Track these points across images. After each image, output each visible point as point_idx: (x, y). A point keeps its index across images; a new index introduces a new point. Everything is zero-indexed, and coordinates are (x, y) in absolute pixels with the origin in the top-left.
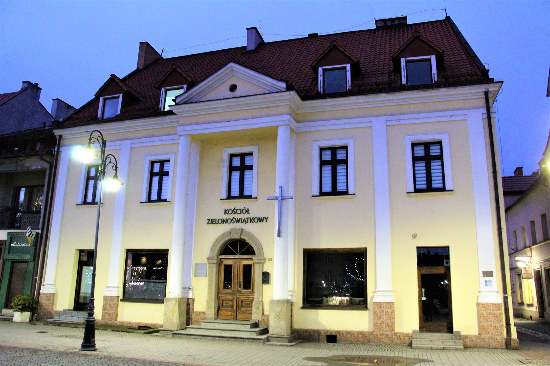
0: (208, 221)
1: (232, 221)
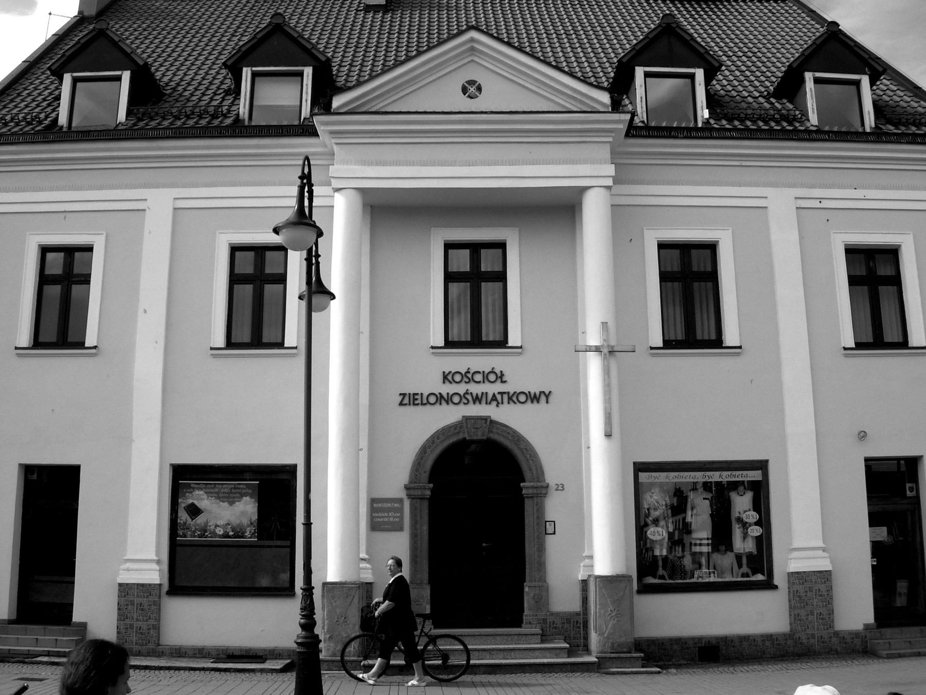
0: (400, 398)
1: (465, 398)
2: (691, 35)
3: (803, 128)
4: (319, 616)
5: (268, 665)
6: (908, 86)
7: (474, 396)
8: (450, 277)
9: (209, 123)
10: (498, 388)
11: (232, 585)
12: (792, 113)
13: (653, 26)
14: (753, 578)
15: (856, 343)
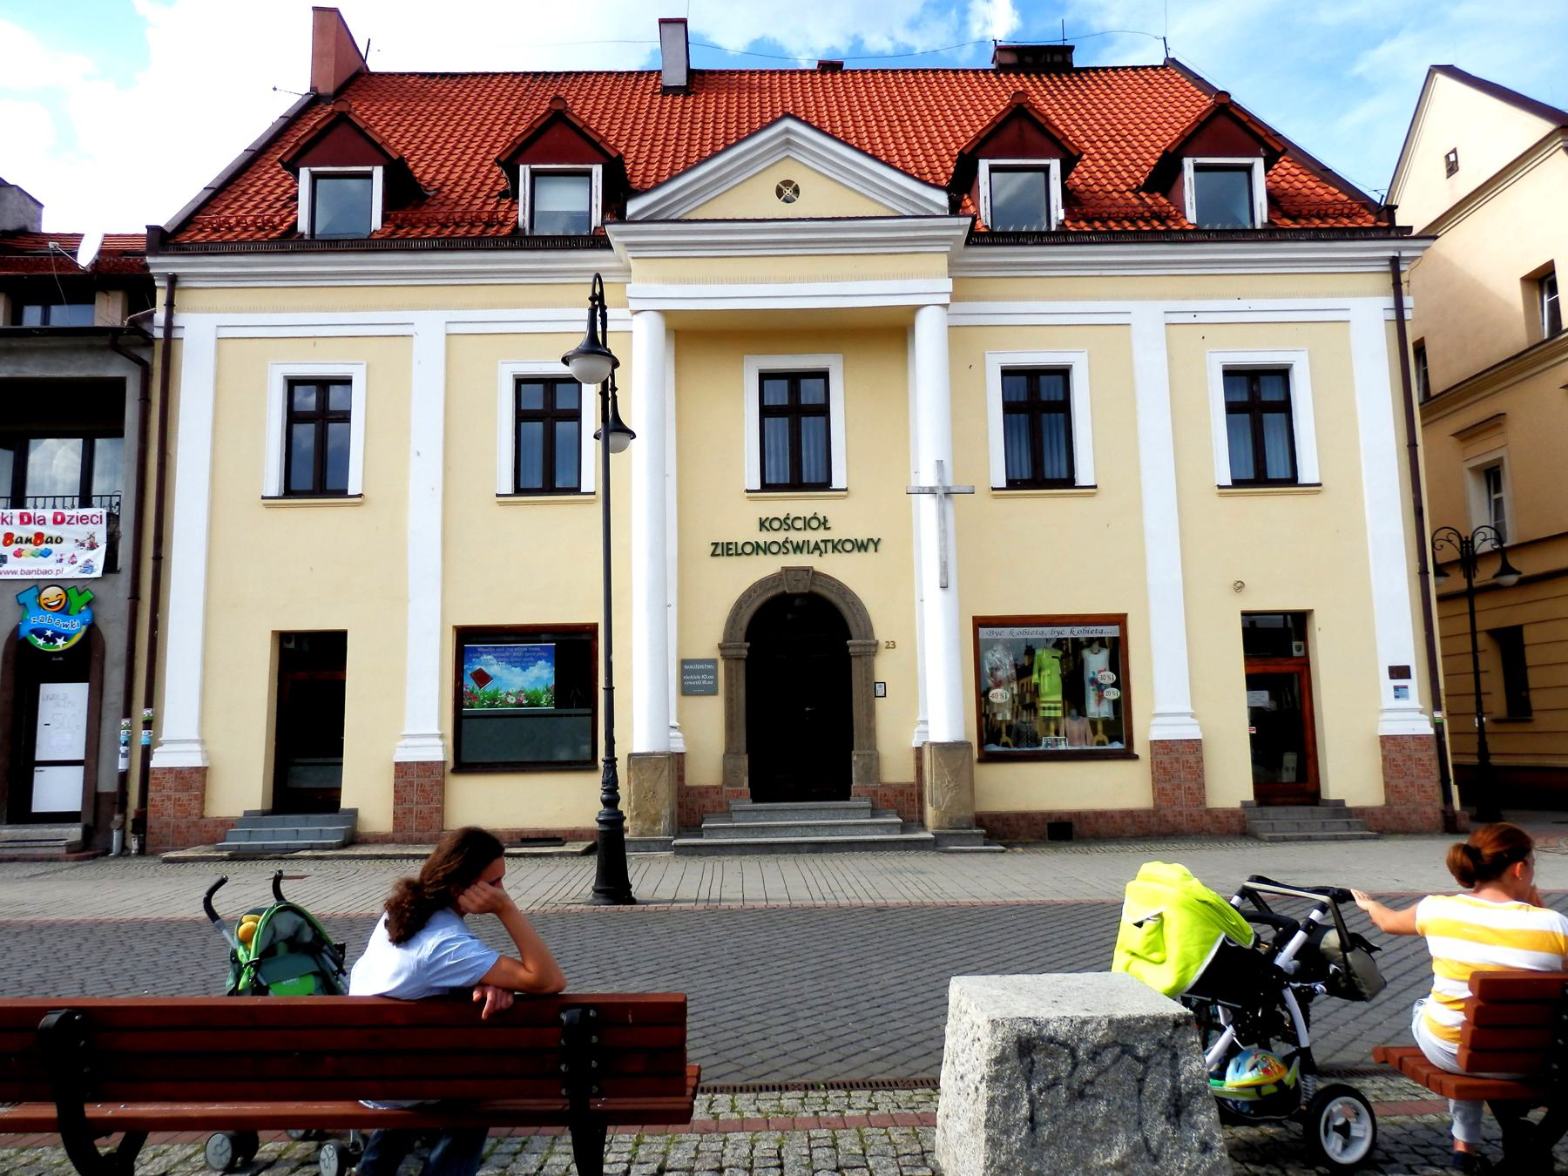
1: (784, 547)
2: (1045, 117)
3: (1177, 228)
4: (623, 790)
5: (567, 848)
6: (1314, 167)
7: (795, 545)
8: (766, 412)
9: (483, 232)
10: (821, 535)
11: (528, 759)
12: (1165, 209)
13: (1002, 107)
14: (1109, 747)
15: (1233, 481)
